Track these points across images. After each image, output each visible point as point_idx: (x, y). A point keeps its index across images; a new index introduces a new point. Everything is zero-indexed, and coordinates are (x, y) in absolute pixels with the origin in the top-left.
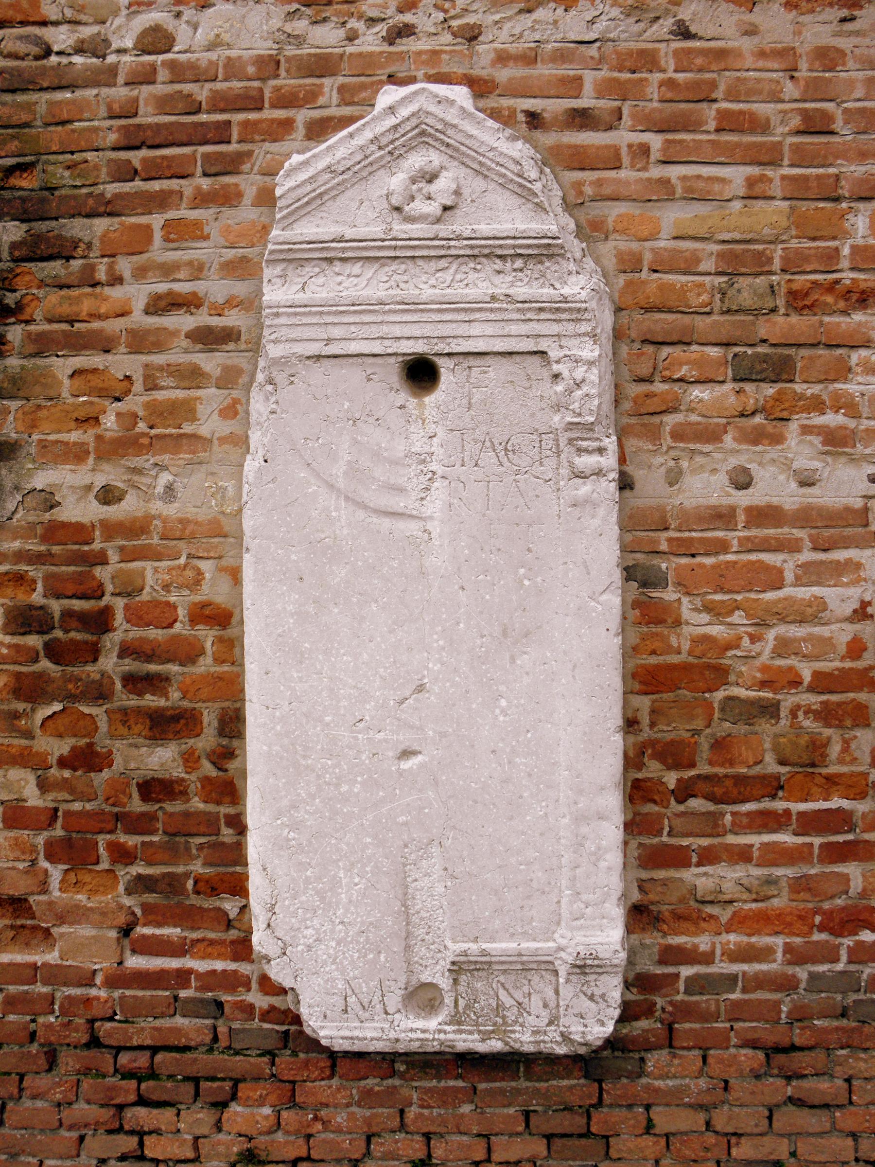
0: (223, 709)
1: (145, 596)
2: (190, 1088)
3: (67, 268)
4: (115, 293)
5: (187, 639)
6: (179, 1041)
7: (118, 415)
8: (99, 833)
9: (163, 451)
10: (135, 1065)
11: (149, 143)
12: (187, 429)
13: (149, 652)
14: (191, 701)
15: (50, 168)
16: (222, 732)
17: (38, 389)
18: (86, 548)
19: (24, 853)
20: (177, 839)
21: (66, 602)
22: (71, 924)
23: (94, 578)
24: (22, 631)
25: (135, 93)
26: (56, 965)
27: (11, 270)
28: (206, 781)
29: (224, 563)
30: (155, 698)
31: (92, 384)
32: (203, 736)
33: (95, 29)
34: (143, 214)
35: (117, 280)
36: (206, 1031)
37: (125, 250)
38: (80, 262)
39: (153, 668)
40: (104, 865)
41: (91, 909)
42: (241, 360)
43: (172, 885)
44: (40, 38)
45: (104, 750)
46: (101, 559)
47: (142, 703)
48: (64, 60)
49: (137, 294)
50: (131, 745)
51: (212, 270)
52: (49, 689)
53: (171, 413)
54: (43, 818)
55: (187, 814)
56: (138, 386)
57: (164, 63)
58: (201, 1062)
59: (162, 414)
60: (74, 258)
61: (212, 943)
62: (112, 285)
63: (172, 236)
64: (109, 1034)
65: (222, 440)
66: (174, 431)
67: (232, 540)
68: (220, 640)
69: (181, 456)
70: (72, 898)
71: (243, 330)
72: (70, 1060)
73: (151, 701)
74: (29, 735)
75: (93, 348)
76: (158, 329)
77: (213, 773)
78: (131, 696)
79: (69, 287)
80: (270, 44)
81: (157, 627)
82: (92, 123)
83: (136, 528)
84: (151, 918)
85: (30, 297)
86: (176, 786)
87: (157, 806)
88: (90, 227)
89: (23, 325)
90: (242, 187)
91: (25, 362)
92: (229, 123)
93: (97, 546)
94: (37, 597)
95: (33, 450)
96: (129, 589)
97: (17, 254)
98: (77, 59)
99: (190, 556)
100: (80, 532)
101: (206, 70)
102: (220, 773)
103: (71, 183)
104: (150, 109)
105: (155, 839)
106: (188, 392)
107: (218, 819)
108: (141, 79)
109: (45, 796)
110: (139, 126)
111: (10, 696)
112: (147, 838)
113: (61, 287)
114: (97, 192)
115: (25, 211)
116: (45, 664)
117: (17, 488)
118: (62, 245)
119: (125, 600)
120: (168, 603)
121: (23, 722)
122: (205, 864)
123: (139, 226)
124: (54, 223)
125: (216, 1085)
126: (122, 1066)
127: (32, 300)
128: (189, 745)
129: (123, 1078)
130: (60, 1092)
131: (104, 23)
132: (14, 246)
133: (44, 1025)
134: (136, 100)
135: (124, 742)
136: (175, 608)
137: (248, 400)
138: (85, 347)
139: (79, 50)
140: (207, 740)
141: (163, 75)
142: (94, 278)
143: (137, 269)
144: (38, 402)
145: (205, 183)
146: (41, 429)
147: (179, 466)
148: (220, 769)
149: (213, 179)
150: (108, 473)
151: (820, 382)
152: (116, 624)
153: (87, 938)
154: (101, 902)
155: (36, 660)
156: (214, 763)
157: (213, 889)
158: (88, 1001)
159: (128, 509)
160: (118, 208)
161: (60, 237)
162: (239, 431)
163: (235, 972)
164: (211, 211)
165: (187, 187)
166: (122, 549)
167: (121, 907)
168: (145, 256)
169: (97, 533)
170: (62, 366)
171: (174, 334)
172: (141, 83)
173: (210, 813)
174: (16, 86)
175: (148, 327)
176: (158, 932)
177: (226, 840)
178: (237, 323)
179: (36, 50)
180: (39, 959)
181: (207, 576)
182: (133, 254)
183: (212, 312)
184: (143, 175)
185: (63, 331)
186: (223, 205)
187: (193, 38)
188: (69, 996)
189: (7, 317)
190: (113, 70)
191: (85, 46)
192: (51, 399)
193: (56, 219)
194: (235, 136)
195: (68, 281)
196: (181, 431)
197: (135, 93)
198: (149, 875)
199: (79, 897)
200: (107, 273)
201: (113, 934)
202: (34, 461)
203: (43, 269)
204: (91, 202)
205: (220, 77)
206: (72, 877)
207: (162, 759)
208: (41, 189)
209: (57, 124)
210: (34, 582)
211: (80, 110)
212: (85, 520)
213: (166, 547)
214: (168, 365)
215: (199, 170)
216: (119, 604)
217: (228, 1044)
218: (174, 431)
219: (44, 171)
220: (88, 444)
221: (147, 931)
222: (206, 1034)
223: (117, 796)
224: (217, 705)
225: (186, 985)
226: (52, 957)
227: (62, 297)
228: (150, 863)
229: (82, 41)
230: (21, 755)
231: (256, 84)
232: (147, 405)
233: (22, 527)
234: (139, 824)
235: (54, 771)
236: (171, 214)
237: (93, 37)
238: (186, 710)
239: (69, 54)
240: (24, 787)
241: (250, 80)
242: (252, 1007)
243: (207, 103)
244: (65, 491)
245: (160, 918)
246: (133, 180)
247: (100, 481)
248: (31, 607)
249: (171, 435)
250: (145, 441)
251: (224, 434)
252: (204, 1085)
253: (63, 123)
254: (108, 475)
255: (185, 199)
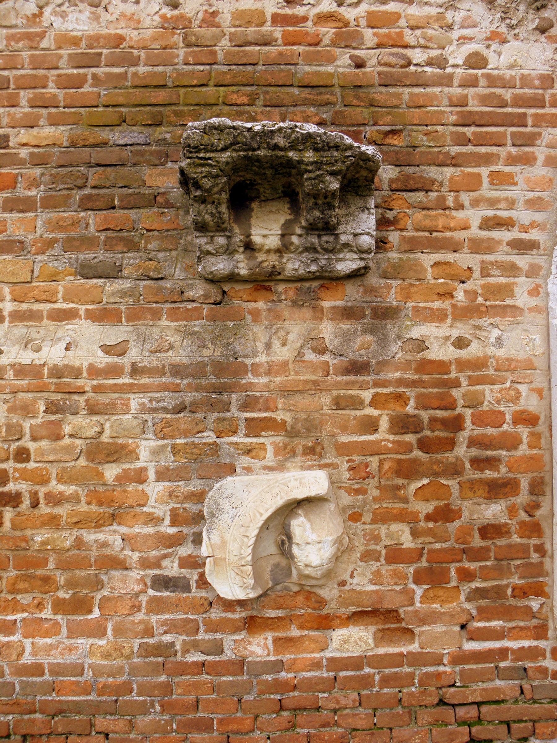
0: (533, 477)
1: (485, 407)
2: (504, 728)
3: (427, 197)
4: (460, 215)
5: (511, 434)
6: (499, 696)
7: (465, 292)
8: (452, 562)
9: (495, 316)
10: (469, 715)
11: (477, 123)
12: (509, 302)
13: (488, 443)
14: (514, 473)
15: (414, 134)
16: (532, 493)
17: (411, 273)
18: (446, 377)
19: (400, 579)
20: (503, 562)
21: (431, 412)
22: (429, 624)
23: (451, 396)
24: (403, 431)
25: (466, 92)
26: (418, 653)
27: (390, 196)
28: (522, 524)
29: (534, 386)
30: (491, 472)
31: (447, 271)
32: (520, 495)
33: (439, 52)
34: (475, 167)
35: (460, 207)
36: (517, 689)
37: (465, 188)
38: (435, 194)
39: (489, 453)
40: (453, 583)
41: (444, 613)
42: (541, 261)
43: (498, 593)
44: (405, 55)
45: (457, 508)
46: (457, 384)
47: (483, 476)
48: (420, 69)
49: (474, 216)
50: (475, 504)
51: (520, 204)
52: (421, 470)
53: (499, 292)
54: (414, 555)
55: (510, 546)
56: (477, 274)
57: (483, 75)
58: (510, 710)
59: (493, 292)
60: (431, 191)
61: (522, 628)
62: (457, 210)
63: (495, 182)
64: (453, 696)
65: (531, 310)
66: (501, 303)
67: (539, 371)
68: (532, 434)
69: (507, 319)
70: (430, 607)
71: (541, 242)
72: (425, 716)
73: (489, 474)
74: (405, 500)
75: (447, 249)
76: (488, 239)
77: (527, 518)
78: (476, 472)
79: (428, 209)
80: (547, 67)
81: (492, 427)
82: (439, 108)
83: (479, 364)
84: (484, 615)
85: (403, 214)
86: (502, 528)
87: (490, 542)
88: (442, 172)
89: (399, 232)
90: (537, 154)
91: (401, 255)
92: (525, 114)
93: (453, 375)
94: (410, 409)
95: (410, 313)
96: (474, 402)
97: (394, 186)
98: (427, 69)
99: (513, 382)
100: (442, 366)
101: (509, 81)
102: (531, 518)
103: (428, 144)
104: (476, 102)
105: (489, 563)
106: (508, 279)
107: (529, 548)
108: (469, 84)
109: (416, 541)
110: (470, 112)
111: (394, 475)
112: (483, 564)
113: (423, 209)
114: (444, 151)
115: (398, 160)
116: (417, 453)
117: (399, 337)
118: (424, 183)
119: (472, 410)
120: (499, 412)
121: (402, 492)
122: (520, 578)
123: (474, 174)
124: (417, 169)
125: (522, 725)
126: (461, 717)
127: (404, 216)
128: (512, 502)
129: (459, 725)
130: (419, 739)
131: (443, 48)
132: (391, 181)
133: (407, 694)
134: (466, 96)
135: (470, 502)
136: (504, 414)
137: (547, 285)
138: (442, 248)
139: (429, 63)
140: (523, 497)
141: (483, 82)
142: (445, 204)
143: (473, 200)
144: (412, 282)
145: (514, 150)
146: (413, 299)
147: (505, 325)
148: (530, 516)
149: (518, 148)
150: (460, 329)
151: (150, 65)
152: (466, 425)
153: (440, 633)
154: (449, 608)
155: (411, 451)
156: (526, 512)
157: (524, 593)
158: (438, 675)
159: (473, 352)
160: (459, 162)
161: (421, 177)
162: (541, 304)
163: (536, 647)
164: (518, 168)
165: (502, 152)
166: (470, 377)
167: (463, 610)
168: (478, 193)
169: (453, 367)
170: (428, 259)
171: (499, 242)
172: (469, 86)
173: (524, 544)
174: (389, 83)
175: (482, 237)
176: (487, 624)
177: (534, 561)
178: (537, 238)
179: (403, 62)
180: (403, 650)
181: (524, 394)
182: (470, 191)
183: (522, 230)
184: (475, 143)
185: (426, 237)
186: (525, 164)
187: (498, 61)
188: (426, 673)
189: (389, 226)
190: (451, 77)
191: (434, 61)
192: (420, 280)
193: (418, 166)
194: (530, 122)
195: (429, 205)
196: (505, 303)
197: (466, 92)
198: (483, 588)
199: (434, 606)
200: (454, 202)
201: (457, 628)
202: (411, 321)
203: (412, 197)
204: (441, 157)
205: (518, 86)
206: (431, 593)
207: (494, 511)
208: (407, 147)
209: (416, 107)
210: (409, 399)
211: (431, 100)
212: (446, 359)
213: (498, 376)
214: (496, 262)
215: (509, 142)
216: (468, 413)
217: (531, 696)
218: (501, 303)
219: (409, 135)
220: (447, 310)
221: (481, 624)
222: (516, 691)
223: (465, 537)
224: (530, 475)
225: (505, 658)
226: (414, 647)
227: (424, 215)
228: (485, 580)
229: (432, 58)
230: (401, 514)
231: (540, 91)
232: (483, 287)
233: (401, 363)
234: (478, 555)
235: (422, 523)
236: (493, 168)
237: (438, 56)
238: (511, 479)
239: (423, 66)
240: (401, 536)
241: (536, 88)
242: (547, 669)
243: (511, 101)
244: (432, 340)
245: (490, 615)
246: (467, 145)
247: (455, 333)
248: (408, 416)
249: (500, 306)
250: (483, 309)
251: (531, 306)
252: (514, 726)
253: (419, 107)
254: (460, 330)
255: (501, 159)
